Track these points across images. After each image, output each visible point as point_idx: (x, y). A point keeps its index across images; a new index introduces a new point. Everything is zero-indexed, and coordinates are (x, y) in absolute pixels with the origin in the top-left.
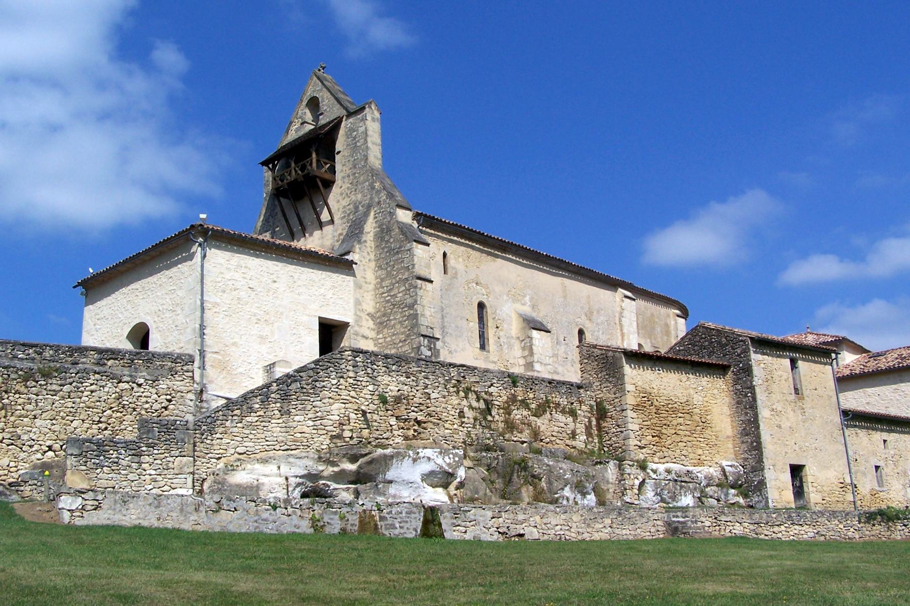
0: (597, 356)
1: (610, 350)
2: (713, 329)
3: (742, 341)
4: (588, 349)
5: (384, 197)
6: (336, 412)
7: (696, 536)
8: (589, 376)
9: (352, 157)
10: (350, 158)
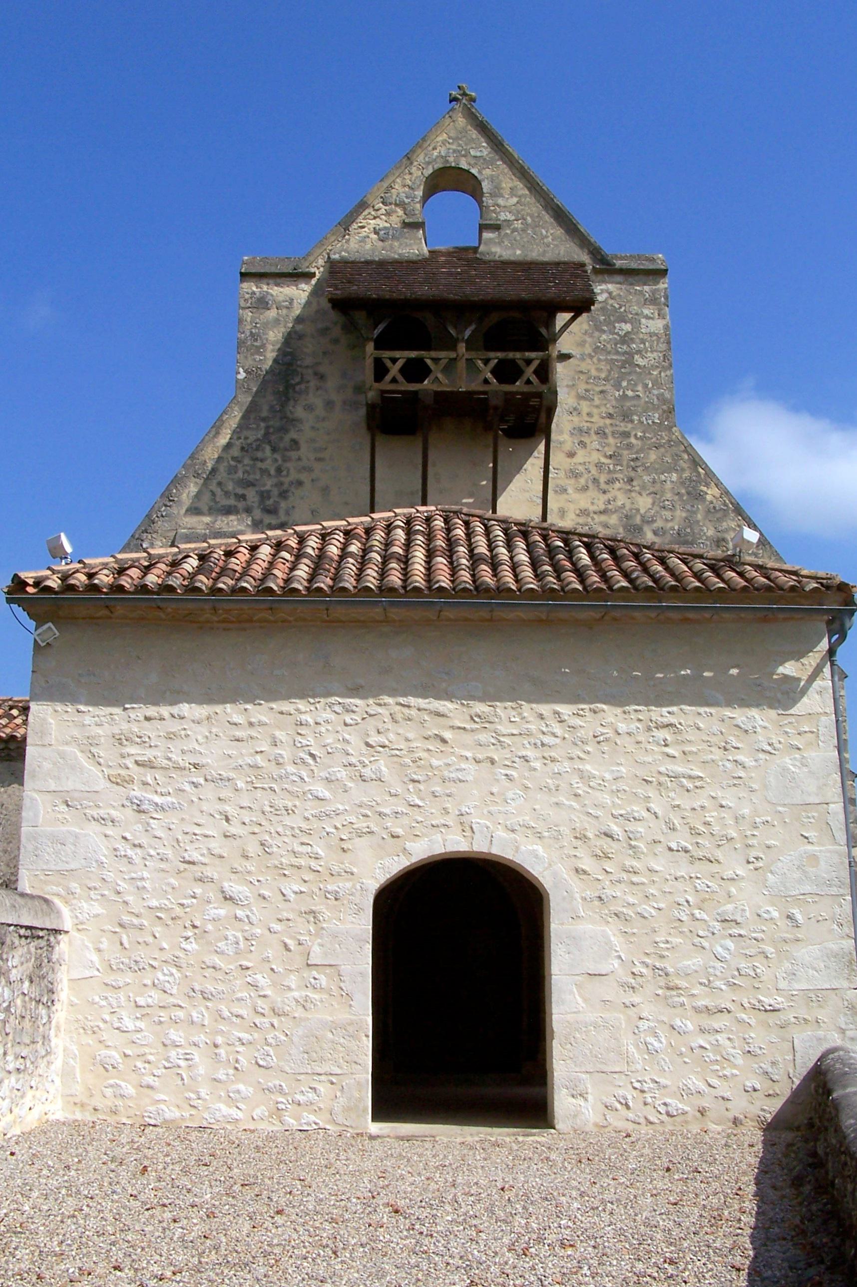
9: (618, 386)
10: (608, 387)
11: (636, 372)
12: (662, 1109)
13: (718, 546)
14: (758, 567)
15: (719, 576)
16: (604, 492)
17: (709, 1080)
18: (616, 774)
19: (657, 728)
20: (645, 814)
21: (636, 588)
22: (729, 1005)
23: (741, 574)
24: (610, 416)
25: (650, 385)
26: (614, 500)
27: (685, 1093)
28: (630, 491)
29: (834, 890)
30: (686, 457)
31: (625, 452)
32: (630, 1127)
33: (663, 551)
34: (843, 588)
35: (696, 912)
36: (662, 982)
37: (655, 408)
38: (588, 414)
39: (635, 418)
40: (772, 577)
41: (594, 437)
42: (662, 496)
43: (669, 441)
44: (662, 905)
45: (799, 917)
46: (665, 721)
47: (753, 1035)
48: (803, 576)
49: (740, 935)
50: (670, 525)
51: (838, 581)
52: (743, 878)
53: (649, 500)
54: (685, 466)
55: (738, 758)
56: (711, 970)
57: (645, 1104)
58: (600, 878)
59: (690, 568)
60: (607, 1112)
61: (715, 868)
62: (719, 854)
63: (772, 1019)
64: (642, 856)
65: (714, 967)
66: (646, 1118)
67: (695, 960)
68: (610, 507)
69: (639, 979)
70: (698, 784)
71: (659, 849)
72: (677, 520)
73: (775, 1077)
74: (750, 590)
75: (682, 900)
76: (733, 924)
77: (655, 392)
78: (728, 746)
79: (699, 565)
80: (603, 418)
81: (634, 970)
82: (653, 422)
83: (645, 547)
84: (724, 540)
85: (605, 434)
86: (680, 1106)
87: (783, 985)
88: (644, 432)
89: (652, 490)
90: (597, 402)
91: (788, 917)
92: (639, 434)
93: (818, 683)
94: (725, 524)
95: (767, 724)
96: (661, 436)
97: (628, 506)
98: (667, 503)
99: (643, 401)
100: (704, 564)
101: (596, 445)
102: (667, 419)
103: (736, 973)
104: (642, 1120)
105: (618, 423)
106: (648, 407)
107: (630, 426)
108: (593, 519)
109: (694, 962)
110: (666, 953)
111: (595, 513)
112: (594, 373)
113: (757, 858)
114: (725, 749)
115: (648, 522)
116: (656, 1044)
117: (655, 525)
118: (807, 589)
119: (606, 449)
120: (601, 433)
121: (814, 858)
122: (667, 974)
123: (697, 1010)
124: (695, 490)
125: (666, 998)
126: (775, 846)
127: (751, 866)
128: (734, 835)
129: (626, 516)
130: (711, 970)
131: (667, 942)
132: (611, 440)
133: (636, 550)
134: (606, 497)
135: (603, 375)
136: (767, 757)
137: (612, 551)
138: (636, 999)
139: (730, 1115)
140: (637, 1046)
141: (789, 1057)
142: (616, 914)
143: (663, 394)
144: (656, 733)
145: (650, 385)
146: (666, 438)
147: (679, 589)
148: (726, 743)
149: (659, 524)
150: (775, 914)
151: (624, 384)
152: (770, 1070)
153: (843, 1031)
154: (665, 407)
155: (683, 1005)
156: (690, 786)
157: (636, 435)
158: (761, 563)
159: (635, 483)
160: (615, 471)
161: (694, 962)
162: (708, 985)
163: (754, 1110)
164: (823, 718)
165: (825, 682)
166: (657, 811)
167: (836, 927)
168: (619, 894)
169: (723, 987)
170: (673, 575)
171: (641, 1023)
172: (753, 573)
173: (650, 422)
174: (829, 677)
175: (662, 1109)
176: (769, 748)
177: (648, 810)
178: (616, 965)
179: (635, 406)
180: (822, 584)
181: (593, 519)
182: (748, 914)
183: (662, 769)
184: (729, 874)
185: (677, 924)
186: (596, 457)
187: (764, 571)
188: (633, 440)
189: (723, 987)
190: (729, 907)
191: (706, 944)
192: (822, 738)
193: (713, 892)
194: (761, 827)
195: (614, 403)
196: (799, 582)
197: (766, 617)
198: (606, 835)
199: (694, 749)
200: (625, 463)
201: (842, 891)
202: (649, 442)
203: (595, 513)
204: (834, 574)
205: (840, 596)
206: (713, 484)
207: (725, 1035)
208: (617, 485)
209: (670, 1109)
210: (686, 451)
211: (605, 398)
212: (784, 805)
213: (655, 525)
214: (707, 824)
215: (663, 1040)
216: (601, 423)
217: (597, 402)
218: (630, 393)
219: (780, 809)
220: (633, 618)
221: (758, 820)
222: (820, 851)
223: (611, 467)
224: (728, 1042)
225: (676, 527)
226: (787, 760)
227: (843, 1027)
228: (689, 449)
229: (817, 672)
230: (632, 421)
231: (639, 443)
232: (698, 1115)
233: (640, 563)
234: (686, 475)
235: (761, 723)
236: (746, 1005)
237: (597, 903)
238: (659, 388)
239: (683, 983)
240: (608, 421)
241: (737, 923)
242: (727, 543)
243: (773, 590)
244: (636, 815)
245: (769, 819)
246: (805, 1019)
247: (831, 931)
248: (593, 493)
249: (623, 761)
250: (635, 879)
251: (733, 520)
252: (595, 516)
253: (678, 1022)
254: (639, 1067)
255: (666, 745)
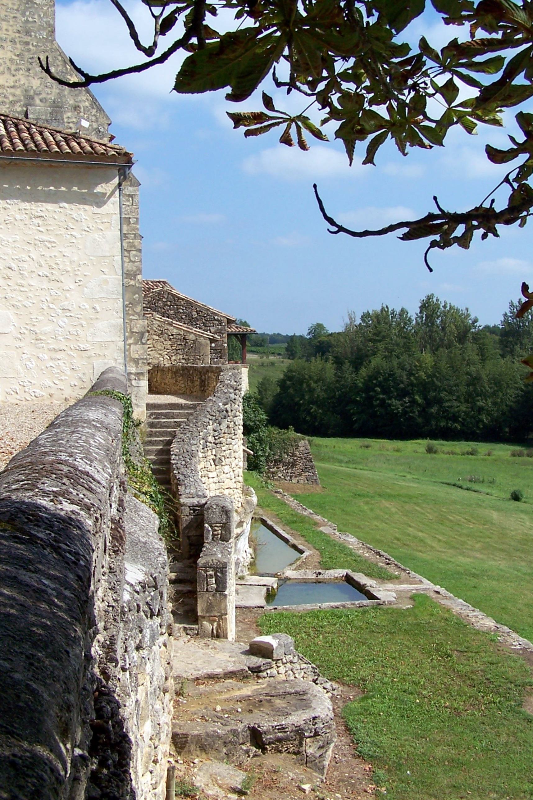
0: (172, 335)
1: (192, 333)
2: (183, 299)
3: (218, 320)
4: (160, 324)
5: (87, 104)
6: (349, 641)
7: (529, 650)
8: (158, 356)
9: (23, 14)
10: (18, 15)
11: (34, 7)
12: (33, 394)
13: (75, 110)
14: (88, 141)
15: (68, 145)
16: (14, 76)
17: (55, 381)
18: (14, 239)
19: (35, 218)
20: (28, 258)
21: (26, 149)
22: (64, 348)
23: (79, 144)
24: (19, 32)
25: (42, 15)
26: (19, 81)
27: (44, 387)
28: (28, 76)
29: (115, 296)
30: (60, 58)
31: (26, 54)
32: (18, 402)
33: (41, 127)
34: (126, 154)
35: (51, 305)
36: (34, 337)
37: (44, 29)
38: (6, 30)
39: (33, 34)
40: (94, 146)
41: (9, 43)
42: (45, 80)
43: (51, 49)
44: (34, 302)
45: (98, 308)
46: (39, 214)
47: (75, 361)
48: (108, 147)
49: (71, 316)
50: (49, 96)
51: (124, 151)
52: (73, 290)
53: (39, 82)
54: (59, 63)
55: (72, 233)
56: (56, 332)
57: (25, 392)
58: (5, 288)
59: (54, 139)
60: (7, 395)
61: (60, 285)
62: (62, 278)
63: (84, 354)
64: (26, 279)
65: (58, 331)
66: (25, 398)
67: (49, 327)
68: (17, 84)
69: (23, 336)
70: (53, 245)
71: (34, 275)
72: (53, 94)
73: (85, 380)
74: (83, 154)
75: (44, 300)
76: (68, 311)
77: (45, 20)
78: (68, 228)
79: (59, 137)
80: (15, 32)
81: (21, 331)
82: (43, 37)
83: (33, 124)
84: (78, 106)
85: (15, 42)
86: (41, 393)
87: (89, 339)
88: (37, 42)
89: (40, 76)
90: (11, 23)
91: (93, 308)
92: (35, 44)
93: (112, 199)
94: (80, 98)
95: (86, 218)
96: (47, 45)
97: (26, 85)
98: (48, 84)
99: (37, 24)
100: (62, 137)
101: (10, 48)
102: (51, 36)
103: (68, 333)
104: (23, 399)
105: (23, 36)
106: (40, 29)
107: (30, 38)
108: (7, 91)
109: (49, 328)
110: (35, 324)
111: (8, 87)
112: (10, 6)
113: (80, 281)
114: (67, 229)
115: (37, 94)
116: (31, 365)
117: (41, 97)
118: (109, 154)
119: (15, 51)
120: (13, 41)
121: (106, 281)
122: (36, 333)
123: (49, 350)
124: (64, 78)
125: (35, 344)
126: (89, 275)
127: (77, 284)
128: (69, 269)
129: (25, 90)
130: (56, 332)
131: (37, 318)
132: (18, 46)
133: (28, 126)
134: (15, 78)
135: (15, 7)
136: (87, 233)
137: (16, 126)
138: (22, 344)
139: (64, 397)
140: (21, 366)
141: (91, 371)
142: (13, 305)
143: (49, 21)
144: (34, 220)
145: (42, 15)
146: (50, 47)
147: (48, 152)
148: (68, 226)
149: (43, 96)
150: (87, 307)
151: (27, 13)
152: (82, 377)
153: (116, 360)
154: (50, 29)
155: (43, 347)
156: (49, 246)
157: (32, 44)
158: (89, 138)
159: (31, 72)
160: (20, 64)
161: (49, 328)
162: (55, 338)
163: (75, 394)
164: (114, 216)
165: (115, 199)
166: (33, 257)
167: (114, 313)
168: (14, 296)
169: (62, 340)
170: (45, 142)
171: (23, 356)
172: (84, 143)
173: (41, 37)
174: (118, 196)
175: (33, 394)
176: (88, 229)
177: (29, 257)
178: (13, 329)
179: (32, 27)
180: (117, 152)
181: (7, 91)
182: (74, 306)
183: (37, 238)
184: (66, 288)
185: (41, 310)
186: (10, 55)
187: (90, 143)
188: (31, 47)
189: (62, 340)
190: (66, 303)
191: (54, 320)
192: (113, 225)
193: (59, 296)
194: (82, 266)
195: (21, 24)
196: (106, 150)
197: (89, 167)
198: (9, 268)
199: (52, 229)
200: (26, 60)
201: (118, 297)
202: (40, 49)
203: (8, 87)
204: (123, 147)
205: (125, 159)
206: (74, 75)
207: (62, 361)
208: (21, 72)
209: (36, 394)
210: (60, 55)
211: (17, 21)
212: (94, 256)
213: (41, 97)
214: (57, 264)
215: (34, 363)
216: (13, 35)
217: (11, 23)
218: (30, 19)
219: (91, 258)
220: (25, 164)
221: (81, 263)
222: (109, 278)
223: (18, 61)
224: (63, 364)
225: (53, 98)
226: (96, 235)
227: (116, 358)
228: (62, 54)
229: (113, 193)
230: (31, 36)
231: (34, 48)
232: (49, 397)
233: (30, 134)
234: (60, 68)
235: (85, 217)
236: (73, 348)
237: (4, 300)
238: (47, 18)
239: (43, 337)
240: (17, 35)
241: (69, 310)
242: (80, 108)
243: (93, 155)
244: (24, 259)
245: (86, 262)
246: (99, 355)
247: (113, 315)
248: (7, 76)
249: (18, 233)
250: (22, 289)
251: (84, 96)
252: (8, 89)
253: (40, 355)
254: (22, 375)
255: (39, 226)
